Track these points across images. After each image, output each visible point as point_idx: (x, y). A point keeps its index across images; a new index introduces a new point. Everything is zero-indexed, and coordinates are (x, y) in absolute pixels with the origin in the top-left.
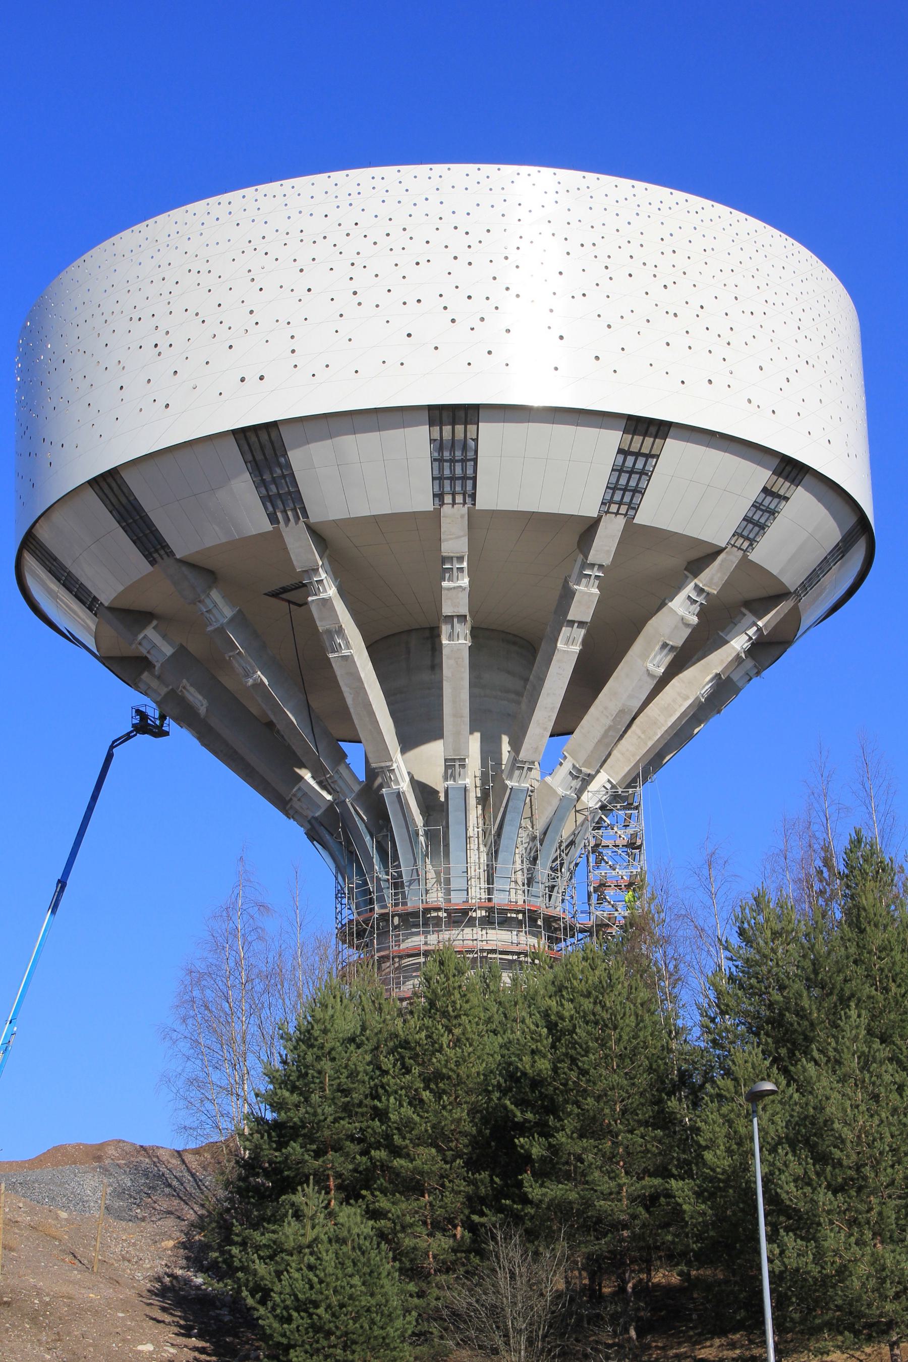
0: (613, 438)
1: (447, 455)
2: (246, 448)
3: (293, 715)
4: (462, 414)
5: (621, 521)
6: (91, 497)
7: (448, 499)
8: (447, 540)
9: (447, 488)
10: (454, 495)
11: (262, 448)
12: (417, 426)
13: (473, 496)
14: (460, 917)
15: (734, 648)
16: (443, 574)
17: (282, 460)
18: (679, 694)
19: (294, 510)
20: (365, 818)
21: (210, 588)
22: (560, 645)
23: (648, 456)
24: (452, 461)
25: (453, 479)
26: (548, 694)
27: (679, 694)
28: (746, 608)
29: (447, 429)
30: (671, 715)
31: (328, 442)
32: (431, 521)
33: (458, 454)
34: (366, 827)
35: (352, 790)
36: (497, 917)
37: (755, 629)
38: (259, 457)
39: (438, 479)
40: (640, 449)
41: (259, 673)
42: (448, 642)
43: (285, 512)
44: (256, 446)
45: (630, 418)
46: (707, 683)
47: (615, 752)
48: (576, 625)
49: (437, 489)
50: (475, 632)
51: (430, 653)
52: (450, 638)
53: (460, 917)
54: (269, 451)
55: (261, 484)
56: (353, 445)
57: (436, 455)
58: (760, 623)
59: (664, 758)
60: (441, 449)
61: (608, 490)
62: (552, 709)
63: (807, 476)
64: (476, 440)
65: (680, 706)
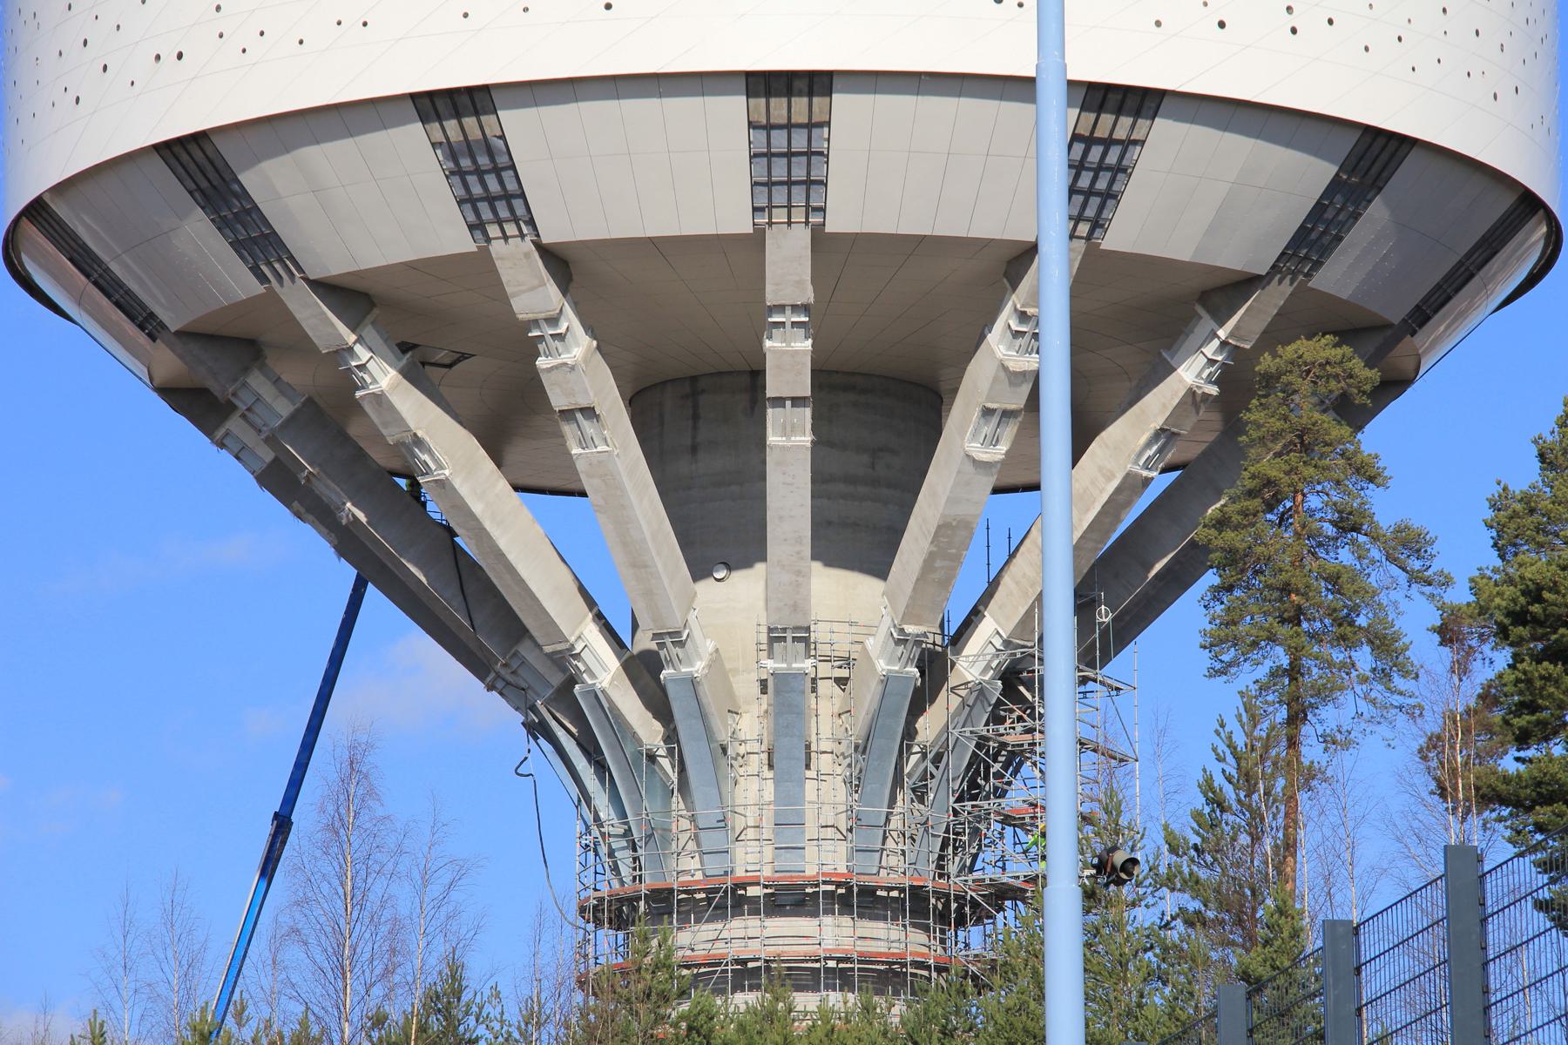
0: (735, 106)
1: (466, 163)
2: (180, 170)
3: (421, 569)
4: (465, 99)
5: (801, 238)
6: (157, 163)
7: (493, 231)
8: (515, 295)
9: (487, 214)
10: (500, 222)
11: (201, 166)
12: (404, 124)
13: (531, 222)
14: (728, 900)
15: (1181, 380)
16: (531, 350)
17: (236, 187)
18: (1100, 469)
19: (280, 260)
20: (574, 730)
21: (246, 370)
22: (773, 438)
23: (810, 126)
24: (480, 173)
25: (491, 200)
26: (781, 518)
27: (1100, 469)
28: (1205, 306)
29: (451, 125)
30: (1088, 510)
31: (287, 158)
32: (480, 267)
33: (484, 161)
34: (579, 744)
35: (548, 684)
36: (791, 899)
37: (1216, 343)
38: (204, 184)
39: (466, 200)
40: (789, 118)
41: (349, 505)
42: (580, 451)
43: (269, 264)
44: (192, 167)
45: (750, 75)
46: (1148, 445)
47: (1006, 580)
48: (788, 403)
49: (472, 218)
50: (756, 376)
51: (690, 423)
52: (583, 443)
53: (728, 900)
54: (212, 175)
55: (222, 224)
56: (328, 158)
57: (451, 165)
58: (1222, 333)
59: (1152, 566)
60: (453, 154)
61: (758, 189)
62: (799, 541)
63: (1165, 101)
64: (503, 137)
65: (1101, 491)
